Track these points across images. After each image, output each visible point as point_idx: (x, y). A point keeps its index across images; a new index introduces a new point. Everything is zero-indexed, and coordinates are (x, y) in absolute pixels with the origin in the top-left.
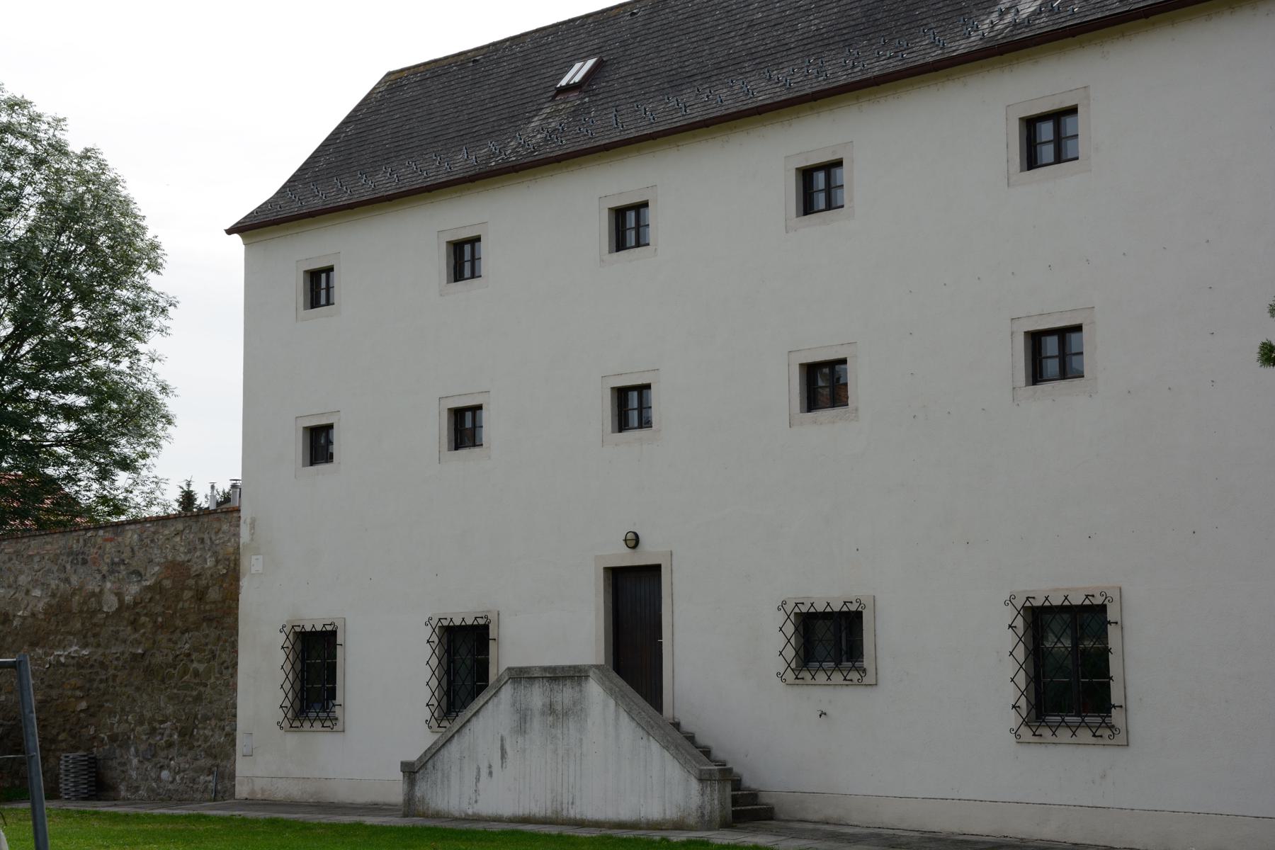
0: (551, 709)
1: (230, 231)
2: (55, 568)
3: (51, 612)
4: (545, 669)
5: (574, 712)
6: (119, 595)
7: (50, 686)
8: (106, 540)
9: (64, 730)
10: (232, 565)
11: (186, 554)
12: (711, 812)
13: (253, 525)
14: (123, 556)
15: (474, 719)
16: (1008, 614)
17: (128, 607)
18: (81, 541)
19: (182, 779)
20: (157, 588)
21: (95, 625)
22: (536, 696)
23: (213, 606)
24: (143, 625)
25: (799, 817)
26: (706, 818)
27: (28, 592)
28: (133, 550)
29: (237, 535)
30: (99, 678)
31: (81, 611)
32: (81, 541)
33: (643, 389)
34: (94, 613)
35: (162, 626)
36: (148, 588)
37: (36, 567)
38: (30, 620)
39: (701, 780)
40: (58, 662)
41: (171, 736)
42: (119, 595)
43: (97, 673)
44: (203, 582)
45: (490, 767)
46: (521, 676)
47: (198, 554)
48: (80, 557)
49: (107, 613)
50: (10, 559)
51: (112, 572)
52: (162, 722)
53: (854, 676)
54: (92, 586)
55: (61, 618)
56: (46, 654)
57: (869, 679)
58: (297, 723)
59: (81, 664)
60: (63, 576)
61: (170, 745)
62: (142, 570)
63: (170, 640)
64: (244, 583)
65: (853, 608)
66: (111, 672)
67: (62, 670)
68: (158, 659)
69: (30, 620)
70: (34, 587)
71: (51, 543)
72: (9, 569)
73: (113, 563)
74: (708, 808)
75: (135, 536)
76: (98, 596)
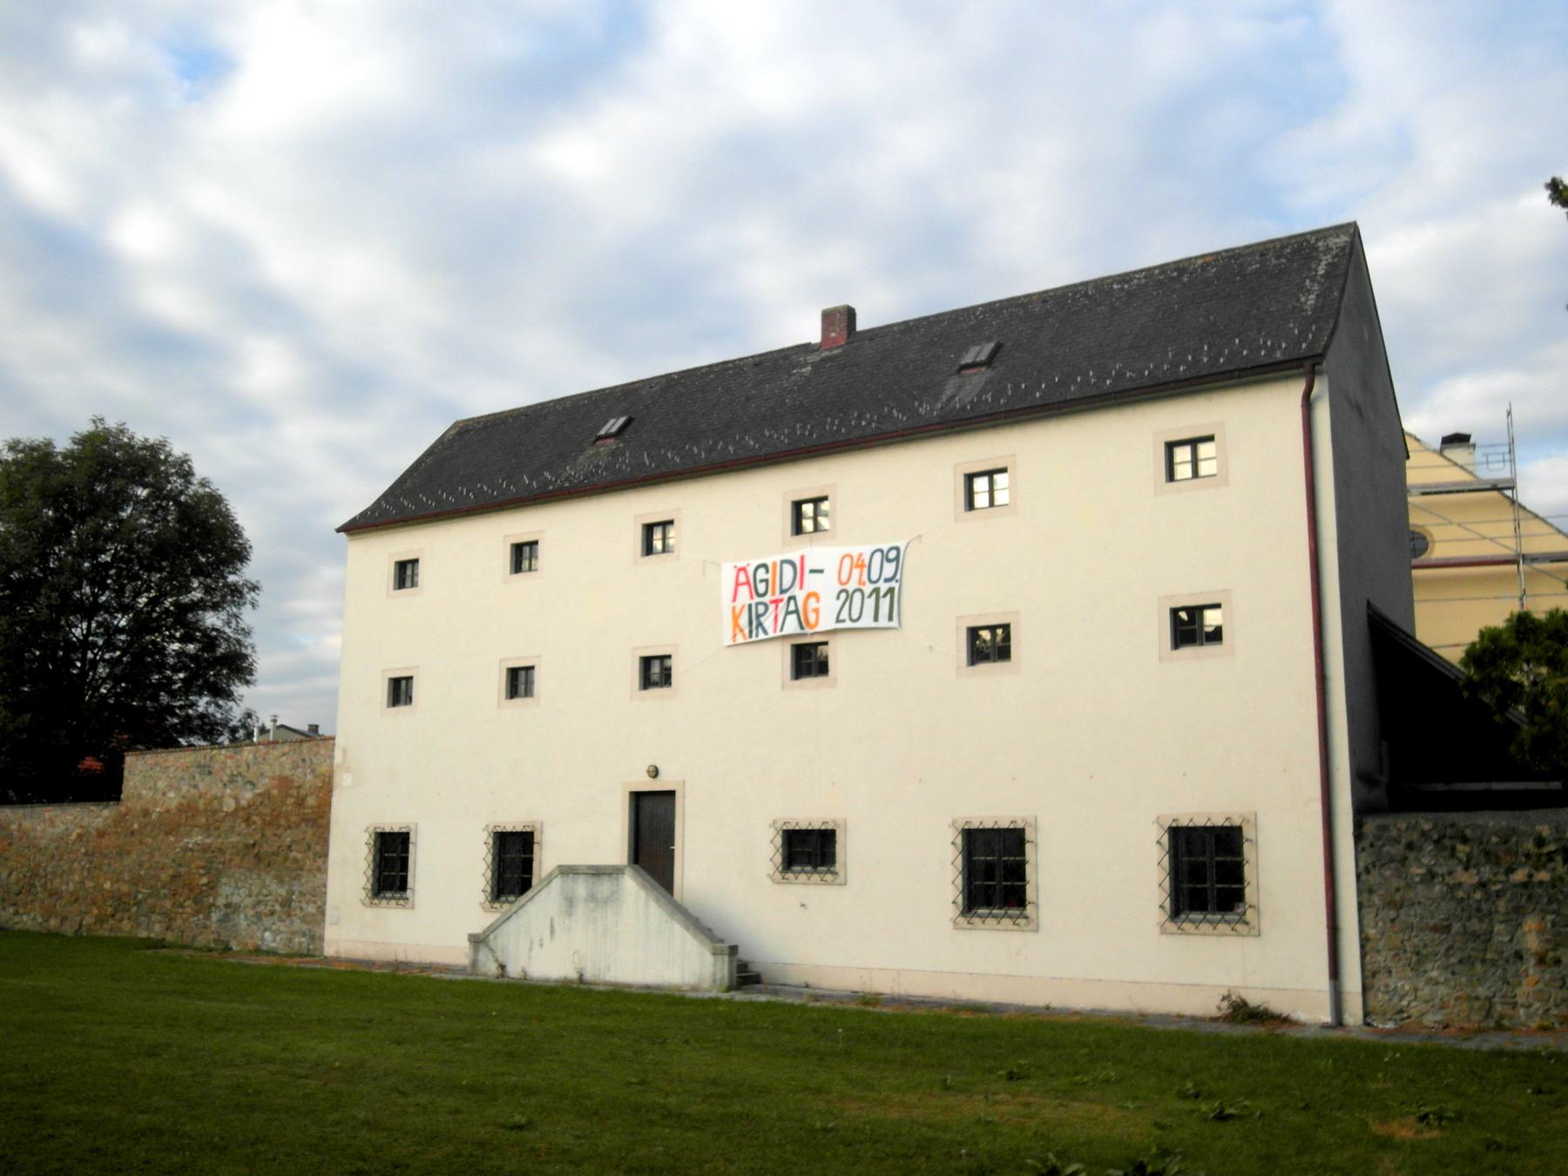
0: (592, 898)
1: (339, 530)
2: (186, 776)
3: (182, 809)
4: (589, 867)
5: (613, 899)
6: (236, 799)
7: (180, 865)
8: (227, 757)
9: (189, 899)
10: (327, 780)
11: (290, 770)
12: (289, 915)
13: (344, 751)
14: (240, 770)
15: (529, 903)
16: (771, 833)
17: (243, 808)
18: (208, 757)
19: (282, 939)
20: (266, 795)
21: (217, 821)
22: (581, 887)
23: (310, 811)
24: (254, 823)
25: (781, 982)
26: (718, 983)
27: (164, 794)
28: (248, 765)
29: (332, 757)
30: (218, 860)
31: (206, 811)
32: (208, 757)
33: (529, 669)
34: (215, 812)
35: (270, 824)
36: (260, 795)
37: (171, 775)
38: (166, 815)
39: (714, 954)
40: (187, 847)
41: (273, 906)
42: (236, 799)
43: (216, 857)
44: (303, 792)
45: (541, 940)
46: (567, 871)
47: (300, 770)
48: (206, 770)
49: (226, 812)
50: (151, 769)
51: (231, 781)
52: (266, 896)
53: (829, 877)
54: (216, 791)
55: (189, 814)
56: (176, 841)
57: (840, 879)
58: (376, 901)
59: (205, 849)
60: (193, 783)
61: (272, 913)
62: (255, 781)
63: (275, 835)
64: (335, 793)
65: (830, 827)
66: (227, 856)
67: (189, 854)
68: (266, 848)
69: (166, 815)
70: (170, 790)
71: (185, 758)
72: (151, 776)
73: (233, 775)
74: (719, 976)
75: (251, 756)
76: (220, 799)
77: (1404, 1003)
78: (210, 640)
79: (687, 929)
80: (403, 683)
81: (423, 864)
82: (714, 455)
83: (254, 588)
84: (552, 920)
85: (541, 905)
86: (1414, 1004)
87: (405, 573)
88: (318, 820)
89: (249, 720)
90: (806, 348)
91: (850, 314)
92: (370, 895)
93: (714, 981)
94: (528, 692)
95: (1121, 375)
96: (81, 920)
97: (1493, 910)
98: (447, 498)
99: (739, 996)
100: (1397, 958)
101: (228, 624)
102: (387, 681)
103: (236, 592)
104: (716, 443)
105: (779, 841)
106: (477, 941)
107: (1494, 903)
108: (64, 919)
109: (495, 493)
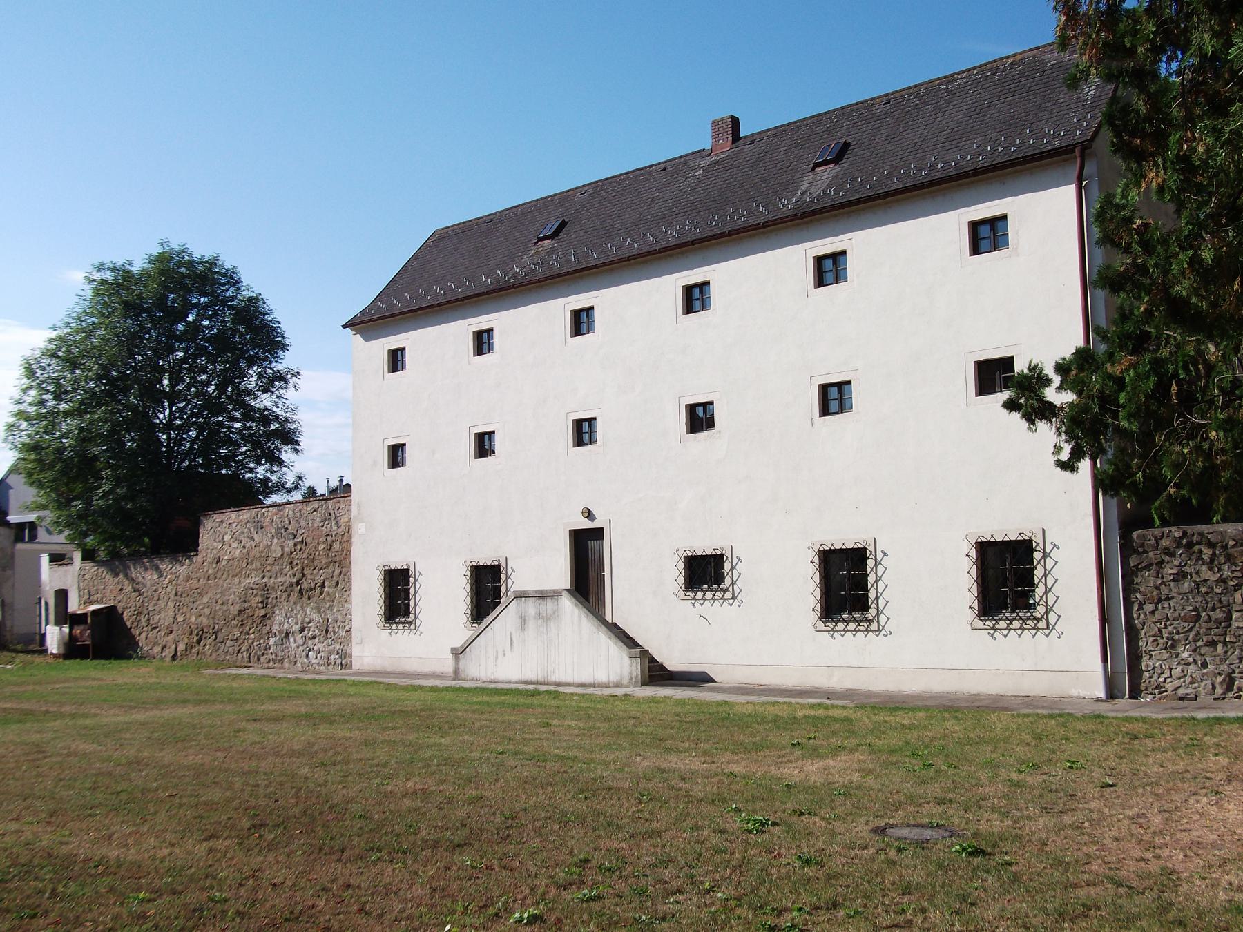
0: (539, 615)
5: (555, 616)
13: (359, 506)
74: (634, 675)
77: (1161, 679)
78: (265, 417)
79: (610, 638)
80: (487, 437)
81: (424, 595)
82: (623, 250)
83: (296, 374)
84: (511, 634)
85: (505, 620)
86: (1168, 680)
87: (396, 360)
88: (339, 560)
89: (300, 482)
90: (699, 153)
91: (735, 122)
92: (383, 619)
93: (631, 679)
94: (592, 440)
95: (934, 166)
96: (176, 648)
97: (1231, 601)
98: (425, 295)
99: (649, 691)
100: (1155, 643)
101: (276, 405)
102: (473, 437)
103: (281, 377)
104: (625, 240)
105: (681, 566)
106: (457, 653)
107: (1232, 595)
108: (163, 648)
109: (1052, 132)
